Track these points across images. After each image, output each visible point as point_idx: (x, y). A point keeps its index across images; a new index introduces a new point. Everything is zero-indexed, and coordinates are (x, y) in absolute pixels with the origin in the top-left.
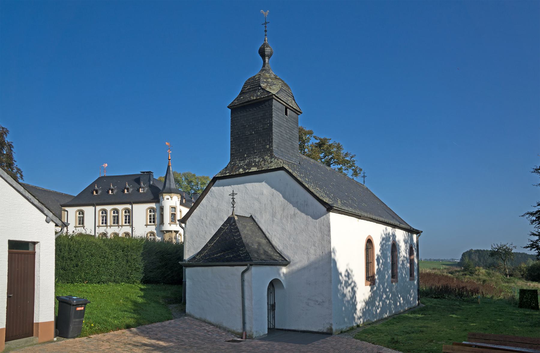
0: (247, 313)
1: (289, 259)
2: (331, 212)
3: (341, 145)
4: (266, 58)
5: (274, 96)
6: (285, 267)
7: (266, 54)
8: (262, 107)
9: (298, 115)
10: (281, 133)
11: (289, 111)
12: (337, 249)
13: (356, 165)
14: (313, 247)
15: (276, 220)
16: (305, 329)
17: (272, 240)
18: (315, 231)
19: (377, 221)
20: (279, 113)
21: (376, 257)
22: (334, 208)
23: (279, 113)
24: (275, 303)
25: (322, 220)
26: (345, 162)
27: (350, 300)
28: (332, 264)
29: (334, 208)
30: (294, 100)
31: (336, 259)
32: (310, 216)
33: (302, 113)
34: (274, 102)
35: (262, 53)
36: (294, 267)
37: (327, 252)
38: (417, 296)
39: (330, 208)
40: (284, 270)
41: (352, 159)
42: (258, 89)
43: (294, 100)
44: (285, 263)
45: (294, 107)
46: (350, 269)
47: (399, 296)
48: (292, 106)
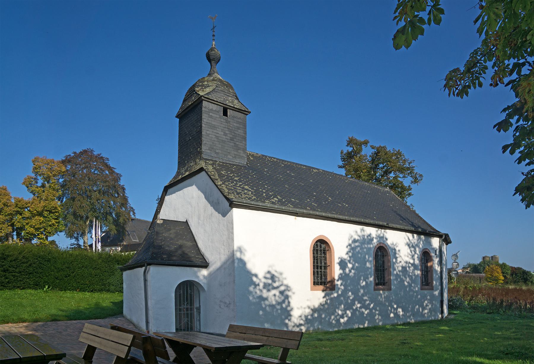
0: (150, 313)
1: (209, 261)
2: (233, 208)
3: (400, 152)
4: (212, 63)
5: (203, 98)
6: (206, 269)
7: (211, 58)
8: (196, 111)
9: (247, 115)
10: (217, 135)
11: (229, 112)
12: (245, 246)
13: (415, 172)
14: (223, 247)
15: (201, 222)
16: (219, 333)
17: (199, 243)
18: (224, 229)
19: (343, 221)
20: (213, 115)
21: (337, 260)
22: (234, 203)
23: (213, 115)
24: (200, 306)
25: (228, 217)
26: (402, 170)
27: (276, 304)
28: (510, 287)
29: (234, 203)
30: (237, 99)
31: (246, 258)
32: (221, 214)
33: (250, 112)
34: (205, 103)
35: (209, 58)
36: (213, 268)
37: (231, 251)
38: (440, 309)
39: (232, 204)
40: (204, 272)
41: (411, 165)
42: (194, 93)
43: (237, 99)
44: (205, 265)
45: (235, 107)
46: (276, 271)
47: (395, 306)
48: (233, 106)
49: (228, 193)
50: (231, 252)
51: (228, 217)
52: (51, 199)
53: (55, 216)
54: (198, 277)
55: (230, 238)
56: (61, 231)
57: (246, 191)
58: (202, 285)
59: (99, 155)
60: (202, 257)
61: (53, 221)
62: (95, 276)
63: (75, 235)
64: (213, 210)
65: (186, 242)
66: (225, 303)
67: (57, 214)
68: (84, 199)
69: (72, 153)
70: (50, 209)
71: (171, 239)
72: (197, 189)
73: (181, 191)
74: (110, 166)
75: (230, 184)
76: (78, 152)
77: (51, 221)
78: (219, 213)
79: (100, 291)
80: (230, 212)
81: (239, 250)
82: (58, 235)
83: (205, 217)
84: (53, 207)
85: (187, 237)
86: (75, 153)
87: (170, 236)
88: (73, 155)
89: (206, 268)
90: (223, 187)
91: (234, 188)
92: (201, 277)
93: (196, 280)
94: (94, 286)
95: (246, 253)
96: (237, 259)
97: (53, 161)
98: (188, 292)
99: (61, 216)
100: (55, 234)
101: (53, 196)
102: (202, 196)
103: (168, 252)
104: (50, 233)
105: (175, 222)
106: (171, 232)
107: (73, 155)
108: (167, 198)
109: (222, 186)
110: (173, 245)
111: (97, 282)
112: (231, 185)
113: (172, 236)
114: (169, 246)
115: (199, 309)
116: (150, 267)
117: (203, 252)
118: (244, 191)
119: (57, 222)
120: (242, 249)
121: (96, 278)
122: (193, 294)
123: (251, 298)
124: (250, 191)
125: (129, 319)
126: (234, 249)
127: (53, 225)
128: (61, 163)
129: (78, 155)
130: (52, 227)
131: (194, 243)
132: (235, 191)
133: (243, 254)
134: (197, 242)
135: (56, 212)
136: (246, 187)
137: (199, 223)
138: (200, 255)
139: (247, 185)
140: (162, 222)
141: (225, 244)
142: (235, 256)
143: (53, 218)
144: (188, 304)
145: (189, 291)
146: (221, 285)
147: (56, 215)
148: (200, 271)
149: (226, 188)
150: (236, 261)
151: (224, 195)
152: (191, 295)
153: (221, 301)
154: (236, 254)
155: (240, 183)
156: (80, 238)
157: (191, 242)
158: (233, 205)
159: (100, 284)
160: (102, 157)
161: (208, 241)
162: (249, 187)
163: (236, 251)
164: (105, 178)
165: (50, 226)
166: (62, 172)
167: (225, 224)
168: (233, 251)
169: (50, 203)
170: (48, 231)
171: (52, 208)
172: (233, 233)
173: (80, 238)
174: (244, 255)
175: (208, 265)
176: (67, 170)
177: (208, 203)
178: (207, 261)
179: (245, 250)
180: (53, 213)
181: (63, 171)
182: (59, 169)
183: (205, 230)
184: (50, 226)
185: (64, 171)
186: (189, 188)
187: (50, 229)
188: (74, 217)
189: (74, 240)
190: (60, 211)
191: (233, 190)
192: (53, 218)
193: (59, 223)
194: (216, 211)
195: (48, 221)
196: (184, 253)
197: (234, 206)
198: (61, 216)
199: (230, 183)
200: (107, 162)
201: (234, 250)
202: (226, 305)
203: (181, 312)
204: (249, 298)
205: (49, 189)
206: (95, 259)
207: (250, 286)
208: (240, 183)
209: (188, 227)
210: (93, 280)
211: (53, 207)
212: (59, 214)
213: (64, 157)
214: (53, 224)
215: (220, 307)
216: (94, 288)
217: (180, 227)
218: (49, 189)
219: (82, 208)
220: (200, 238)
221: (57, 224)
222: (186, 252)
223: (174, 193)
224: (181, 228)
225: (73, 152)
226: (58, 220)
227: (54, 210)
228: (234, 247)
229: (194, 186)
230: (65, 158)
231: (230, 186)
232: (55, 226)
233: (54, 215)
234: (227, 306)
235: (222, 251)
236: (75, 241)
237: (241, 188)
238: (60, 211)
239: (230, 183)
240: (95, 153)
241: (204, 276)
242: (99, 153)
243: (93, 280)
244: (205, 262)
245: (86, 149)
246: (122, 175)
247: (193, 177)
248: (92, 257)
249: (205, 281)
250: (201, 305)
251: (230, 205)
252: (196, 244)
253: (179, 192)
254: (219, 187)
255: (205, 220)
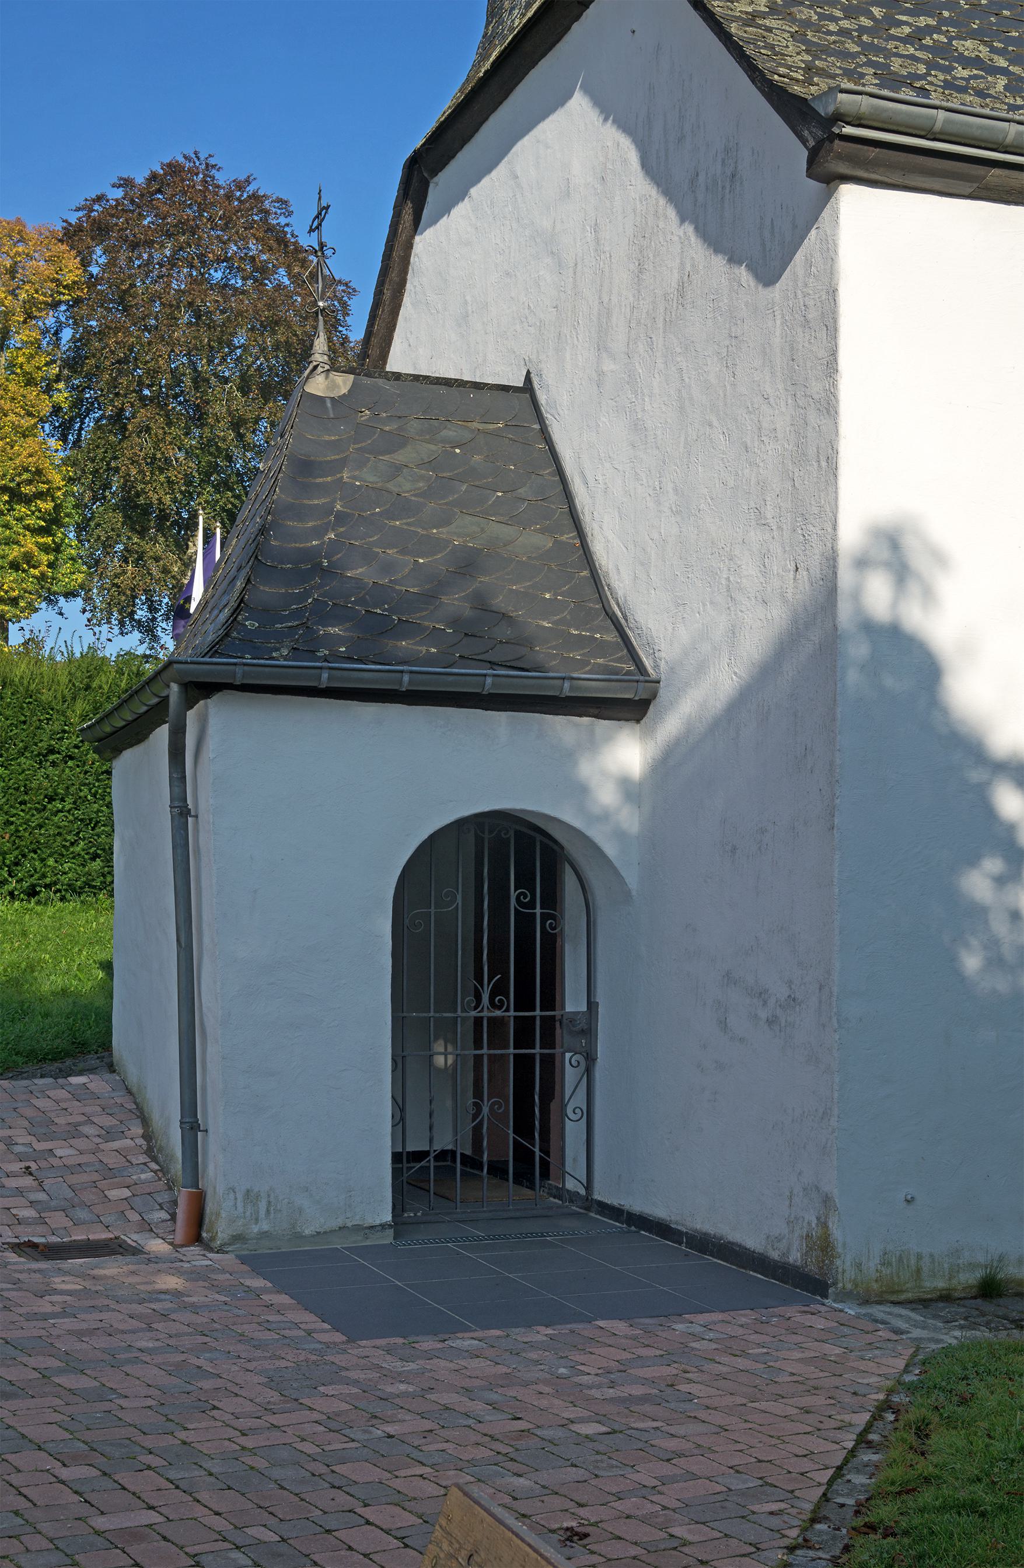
1: (656, 667)
6: (637, 727)
14: (755, 536)
15: (612, 367)
17: (596, 531)
22: (848, 130)
24: (592, 1005)
25: (800, 272)
29: (848, 130)
37: (815, 561)
49: (809, 69)
50: (816, 571)
51: (800, 272)
52: (15, 428)
53: (38, 518)
54: (581, 791)
55: (811, 451)
56: (70, 594)
57: (961, 72)
58: (610, 850)
59: (240, 186)
60: (612, 637)
61: (30, 543)
62: (51, 800)
63: (141, 614)
64: (697, 250)
65: (506, 532)
66: (762, 995)
67: (47, 506)
68: (169, 424)
69: (114, 186)
70: (12, 480)
71: (401, 507)
72: (593, 116)
73: (500, 172)
74: (296, 243)
75: (835, 19)
76: (140, 180)
77: (17, 543)
78: (734, 260)
79: (80, 894)
80: (813, 232)
81: (885, 554)
82: (61, 614)
83: (639, 323)
84: (26, 470)
85: (522, 492)
86: (126, 183)
87: (390, 486)
88: (119, 193)
89: (638, 721)
90: (769, 30)
91: (860, 43)
92: (607, 796)
93: (568, 815)
94: (43, 860)
95: (947, 587)
96: (869, 628)
97: (20, 232)
98: (509, 898)
99: (68, 515)
100: (36, 610)
101: (23, 412)
102: (625, 161)
103: (360, 601)
104: (14, 602)
105: (443, 390)
106: (401, 457)
107: (119, 193)
108: (424, 244)
109: (759, 26)
110: (403, 552)
111: (59, 839)
112: (845, 24)
113: (405, 486)
114: (368, 557)
115: (583, 1032)
116: (206, 706)
117: (620, 594)
118: (948, 70)
119: (45, 549)
120: (911, 544)
121: (55, 814)
122: (544, 917)
123: (972, 962)
124: (1004, 71)
125: (134, 1090)
126: (834, 539)
127: (28, 563)
128: (61, 241)
129: (142, 195)
130: (24, 571)
131: (569, 537)
132: (870, 63)
133: (913, 587)
134: (588, 530)
135: (40, 495)
136: (969, 43)
137: (601, 374)
138: (601, 619)
139: (973, 35)
140: (344, 390)
141: (769, 512)
142: (845, 612)
143: (27, 528)
144: (499, 989)
145: (513, 896)
146: (734, 849)
147: (40, 511)
148: (593, 745)
149: (798, 37)
150: (859, 650)
151: (770, 82)
152: (525, 922)
153: (729, 979)
154: (856, 595)
155: (923, 21)
156: (164, 625)
157: (542, 531)
158: (840, 157)
159: (77, 849)
160: (255, 197)
161: (658, 503)
162: (993, 50)
163: (862, 563)
164: (269, 307)
165: (15, 566)
166: (64, 287)
167: (777, 341)
168: (831, 560)
169: (12, 447)
170: (6, 592)
171: (20, 475)
172: (829, 407)
173: (164, 625)
174: (929, 595)
175: (654, 695)
176: (92, 282)
177: (662, 201)
178: (648, 663)
179: (940, 558)
180: (27, 500)
181: (69, 279)
182: (49, 271)
183: (637, 427)
184: (15, 566)
185: (74, 282)
186: (548, 129)
187: (15, 581)
188: (124, 517)
189: (137, 635)
190: (59, 489)
191: (854, 56)
192: (27, 528)
193: (57, 549)
194: (717, 251)
195: (6, 544)
196: (481, 603)
197: (843, 169)
198: (68, 515)
199: (839, 14)
200: (283, 220)
201: (834, 550)
202: (763, 1015)
203: (507, 1047)
204: (952, 962)
205: (7, 380)
206: (46, 696)
207: (973, 860)
208: (923, 21)
209: (537, 426)
210: (40, 826)
211: (26, 470)
212: (57, 508)
213: (78, 209)
214: (28, 558)
215: (723, 1025)
216: (44, 876)
217: (475, 425)
218: (7, 380)
219: (161, 470)
220: (606, 491)
221: (45, 558)
222: (499, 602)
223: (462, 195)
224: (485, 432)
225: (116, 181)
226: (54, 535)
227: (29, 482)
228: (835, 528)
229: (579, 103)
230: (81, 214)
231: (831, 33)
232: (35, 567)
233: (33, 513)
234: (771, 1022)
235: (750, 569)
236: (142, 642)
237: (923, 48)
238: (59, 489)
239: (839, 14)
240: (222, 178)
241: (629, 789)
242: (242, 178)
243: (40, 826)
244: (628, 673)
245: (181, 160)
246: (354, 290)
247: (568, 28)
248: (33, 687)
249: (630, 820)
250: (600, 997)
251: (811, 162)
252: (577, 542)
253: (485, 181)
254: (734, 28)
255: (641, 348)
